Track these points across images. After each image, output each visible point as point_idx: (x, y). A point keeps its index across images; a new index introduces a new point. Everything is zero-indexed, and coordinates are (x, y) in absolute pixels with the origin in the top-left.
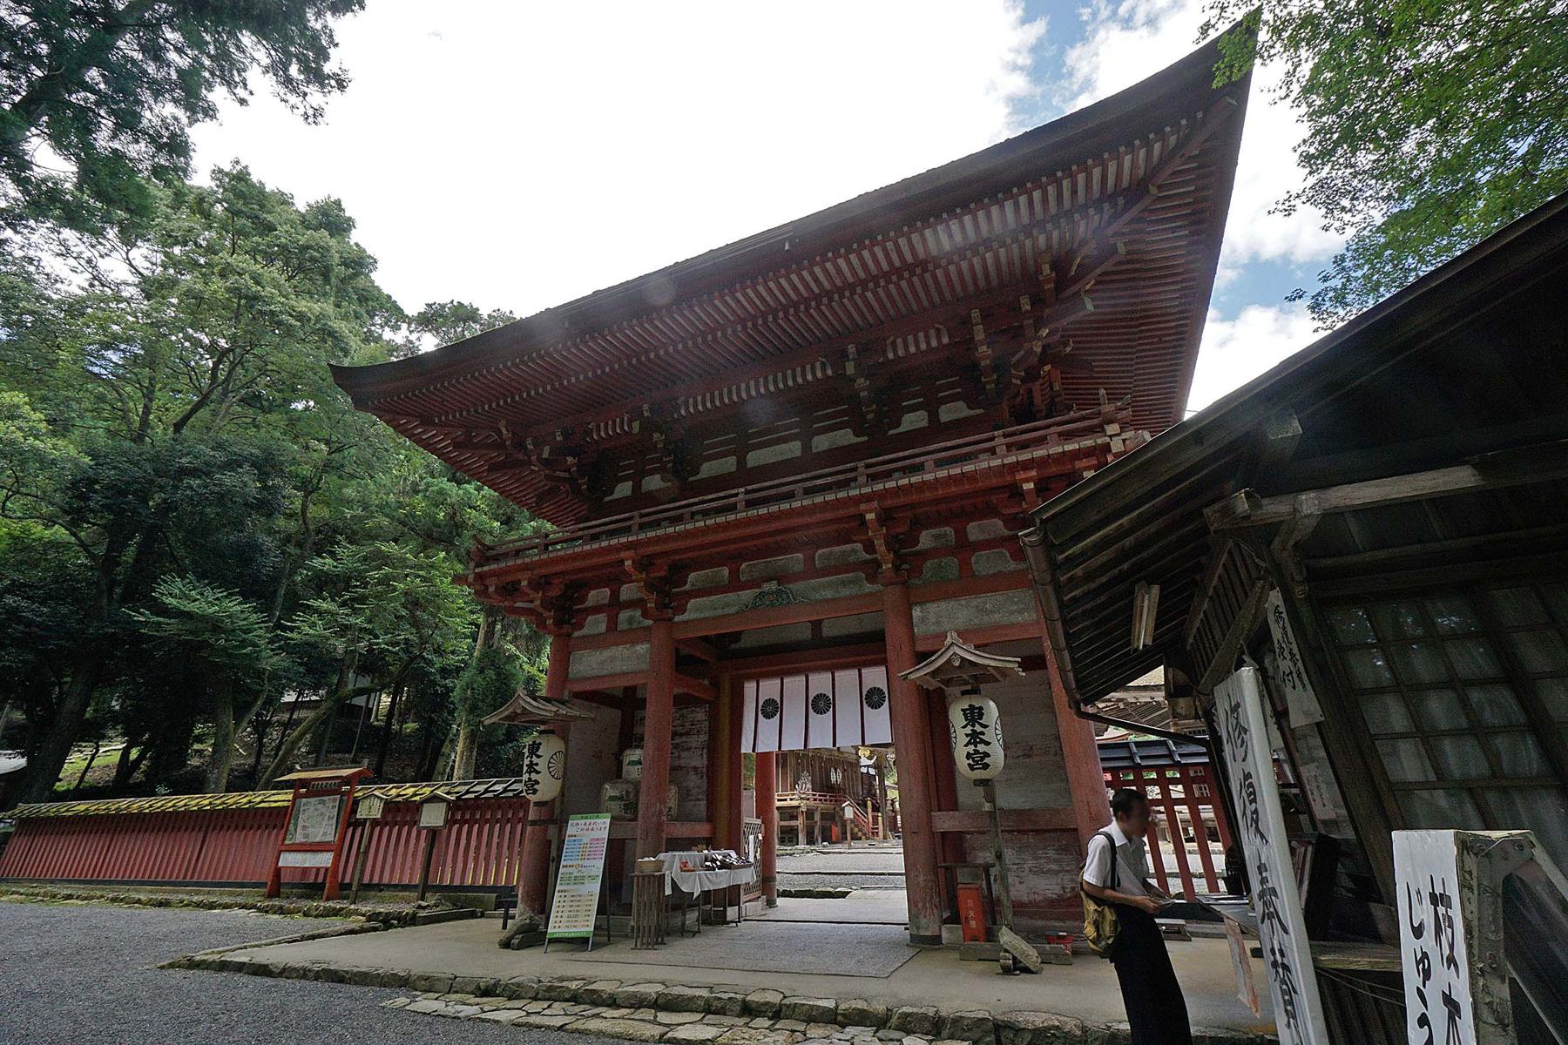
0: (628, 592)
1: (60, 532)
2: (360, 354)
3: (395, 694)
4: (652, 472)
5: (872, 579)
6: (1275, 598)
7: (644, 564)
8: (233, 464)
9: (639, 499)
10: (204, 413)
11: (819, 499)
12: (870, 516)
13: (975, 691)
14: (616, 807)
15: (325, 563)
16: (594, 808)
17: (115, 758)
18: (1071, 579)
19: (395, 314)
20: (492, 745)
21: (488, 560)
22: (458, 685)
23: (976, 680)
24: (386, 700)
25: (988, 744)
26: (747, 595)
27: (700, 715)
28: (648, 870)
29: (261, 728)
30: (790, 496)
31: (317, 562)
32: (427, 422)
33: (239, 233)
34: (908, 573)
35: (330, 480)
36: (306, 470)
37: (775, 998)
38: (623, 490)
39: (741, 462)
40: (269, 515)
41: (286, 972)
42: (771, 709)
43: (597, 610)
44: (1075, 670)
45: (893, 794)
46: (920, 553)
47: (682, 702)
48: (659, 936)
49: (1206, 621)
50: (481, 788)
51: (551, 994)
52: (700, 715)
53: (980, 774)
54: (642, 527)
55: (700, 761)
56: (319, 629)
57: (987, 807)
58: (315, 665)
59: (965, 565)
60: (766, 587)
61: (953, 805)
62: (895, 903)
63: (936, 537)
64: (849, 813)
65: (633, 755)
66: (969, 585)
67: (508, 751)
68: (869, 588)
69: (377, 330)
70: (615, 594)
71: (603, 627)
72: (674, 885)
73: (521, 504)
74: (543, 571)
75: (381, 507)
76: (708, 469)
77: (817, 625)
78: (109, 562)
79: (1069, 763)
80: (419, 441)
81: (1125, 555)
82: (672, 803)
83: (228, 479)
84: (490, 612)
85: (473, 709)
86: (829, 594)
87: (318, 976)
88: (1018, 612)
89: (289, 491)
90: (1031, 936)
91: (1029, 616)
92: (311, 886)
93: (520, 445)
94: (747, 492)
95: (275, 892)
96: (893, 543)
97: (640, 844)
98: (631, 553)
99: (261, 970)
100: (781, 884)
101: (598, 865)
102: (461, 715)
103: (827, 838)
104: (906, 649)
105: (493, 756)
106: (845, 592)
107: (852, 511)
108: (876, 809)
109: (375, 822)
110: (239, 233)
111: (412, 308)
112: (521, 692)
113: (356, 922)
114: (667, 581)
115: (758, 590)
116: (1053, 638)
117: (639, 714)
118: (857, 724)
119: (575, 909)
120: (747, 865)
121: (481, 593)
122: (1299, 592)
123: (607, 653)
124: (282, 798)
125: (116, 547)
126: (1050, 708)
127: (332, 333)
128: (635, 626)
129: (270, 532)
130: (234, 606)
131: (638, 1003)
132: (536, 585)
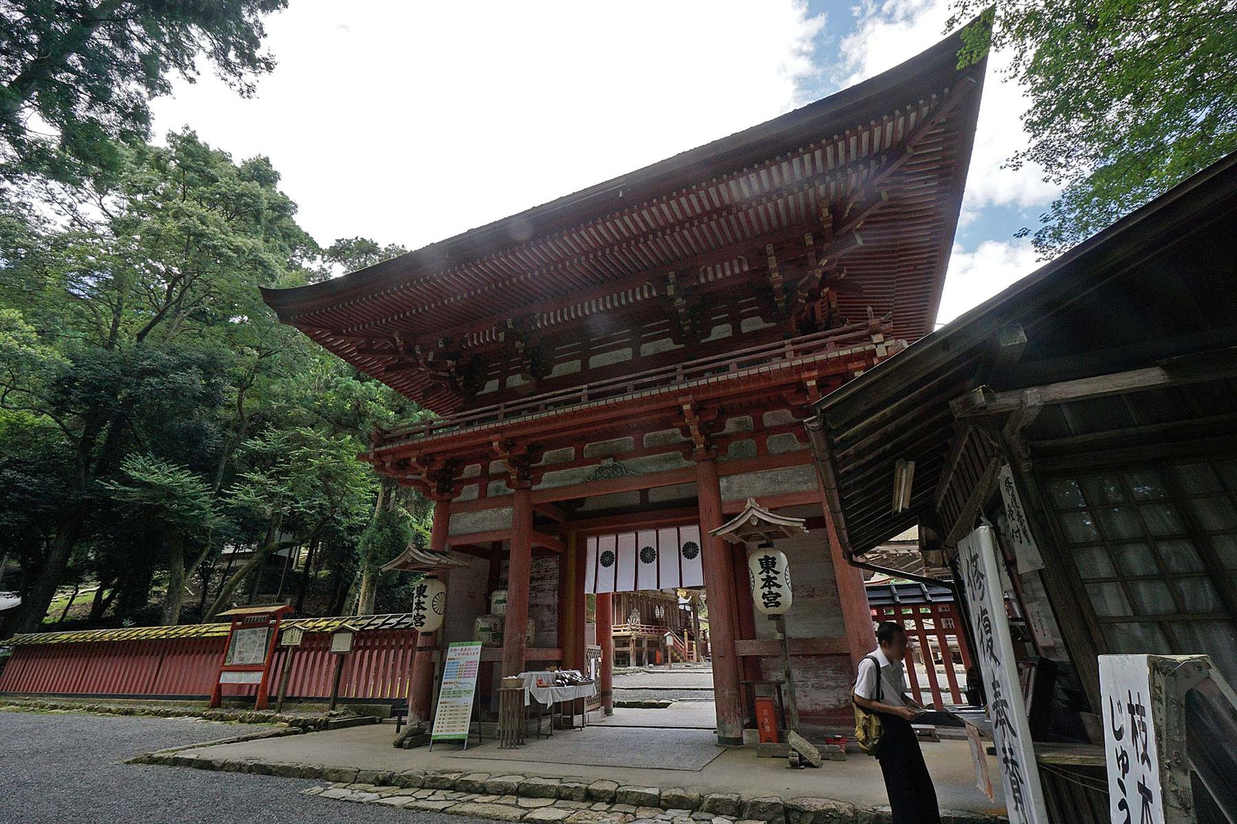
0: (495, 466)
1: (47, 420)
2: (284, 279)
3: (312, 547)
4: (514, 372)
5: (688, 456)
6: (1006, 472)
7: (508, 445)
8: (184, 366)
9: (504, 394)
10: (161, 326)
11: (646, 394)
12: (687, 407)
13: (769, 545)
14: (486, 636)
15: (256, 444)
16: (469, 637)
17: (91, 598)
18: (845, 457)
19: (311, 247)
20: (388, 588)
21: (385, 442)
22: (361, 540)
23: (770, 536)
24: (304, 552)
25: (779, 586)
26: (589, 469)
27: (552, 564)
28: (511, 686)
29: (206, 574)
30: (623, 391)
31: (250, 443)
32: (337, 333)
33: (189, 183)
34: (716, 452)
35: (260, 379)
36: (241, 371)
37: (611, 787)
38: (492, 386)
39: (585, 364)
40: (213, 406)
41: (226, 767)
42: (608, 559)
43: (471, 481)
44: (848, 528)
45: (704, 626)
46: (726, 436)
47: (538, 553)
48: (520, 738)
49: (952, 490)
50: (380, 621)
51: (434, 783)
52: (552, 564)
53: (773, 610)
54: (506, 415)
55: (552, 600)
56: (252, 496)
57: (779, 636)
58: (249, 524)
59: (761, 446)
60: (605, 463)
61: (752, 635)
62: (706, 712)
63: (739, 423)
64: (670, 641)
65: (500, 595)
66: (764, 461)
67: (400, 592)
68: (685, 463)
69: (297, 260)
70: (485, 469)
71: (475, 495)
72: (532, 698)
73: (411, 397)
74: (429, 450)
75: (300, 400)
76: (559, 370)
77: (644, 493)
78: (86, 443)
79: (844, 602)
80: (330, 348)
81: (887, 438)
82: (530, 633)
83: (180, 378)
84: (387, 483)
85: (373, 559)
86: (654, 468)
87: (250, 770)
88: (803, 482)
89: (228, 387)
90: (813, 738)
91: (812, 486)
92: (245, 699)
93: (410, 351)
94: (589, 388)
95: (217, 703)
96: (705, 428)
97: (505, 666)
98: (498, 436)
99: (206, 765)
100: (616, 697)
101: (472, 682)
102: (364, 564)
103: (652, 661)
104: (715, 512)
105: (389, 596)
106: (667, 467)
107: (672, 403)
108: (691, 638)
109: (296, 648)
110: (189, 183)
111: (325, 243)
112: (411, 545)
113: (281, 727)
114: (526, 458)
115: (598, 466)
116: (831, 503)
117: (504, 563)
118: (676, 571)
119: (453, 717)
120: (589, 682)
121: (380, 468)
122: (1025, 466)
123: (479, 515)
124: (223, 629)
125: (92, 431)
126: (829, 558)
127: (262, 263)
128: (501, 493)
129: (213, 419)
130: (185, 478)
131: (503, 791)
132: (422, 461)
